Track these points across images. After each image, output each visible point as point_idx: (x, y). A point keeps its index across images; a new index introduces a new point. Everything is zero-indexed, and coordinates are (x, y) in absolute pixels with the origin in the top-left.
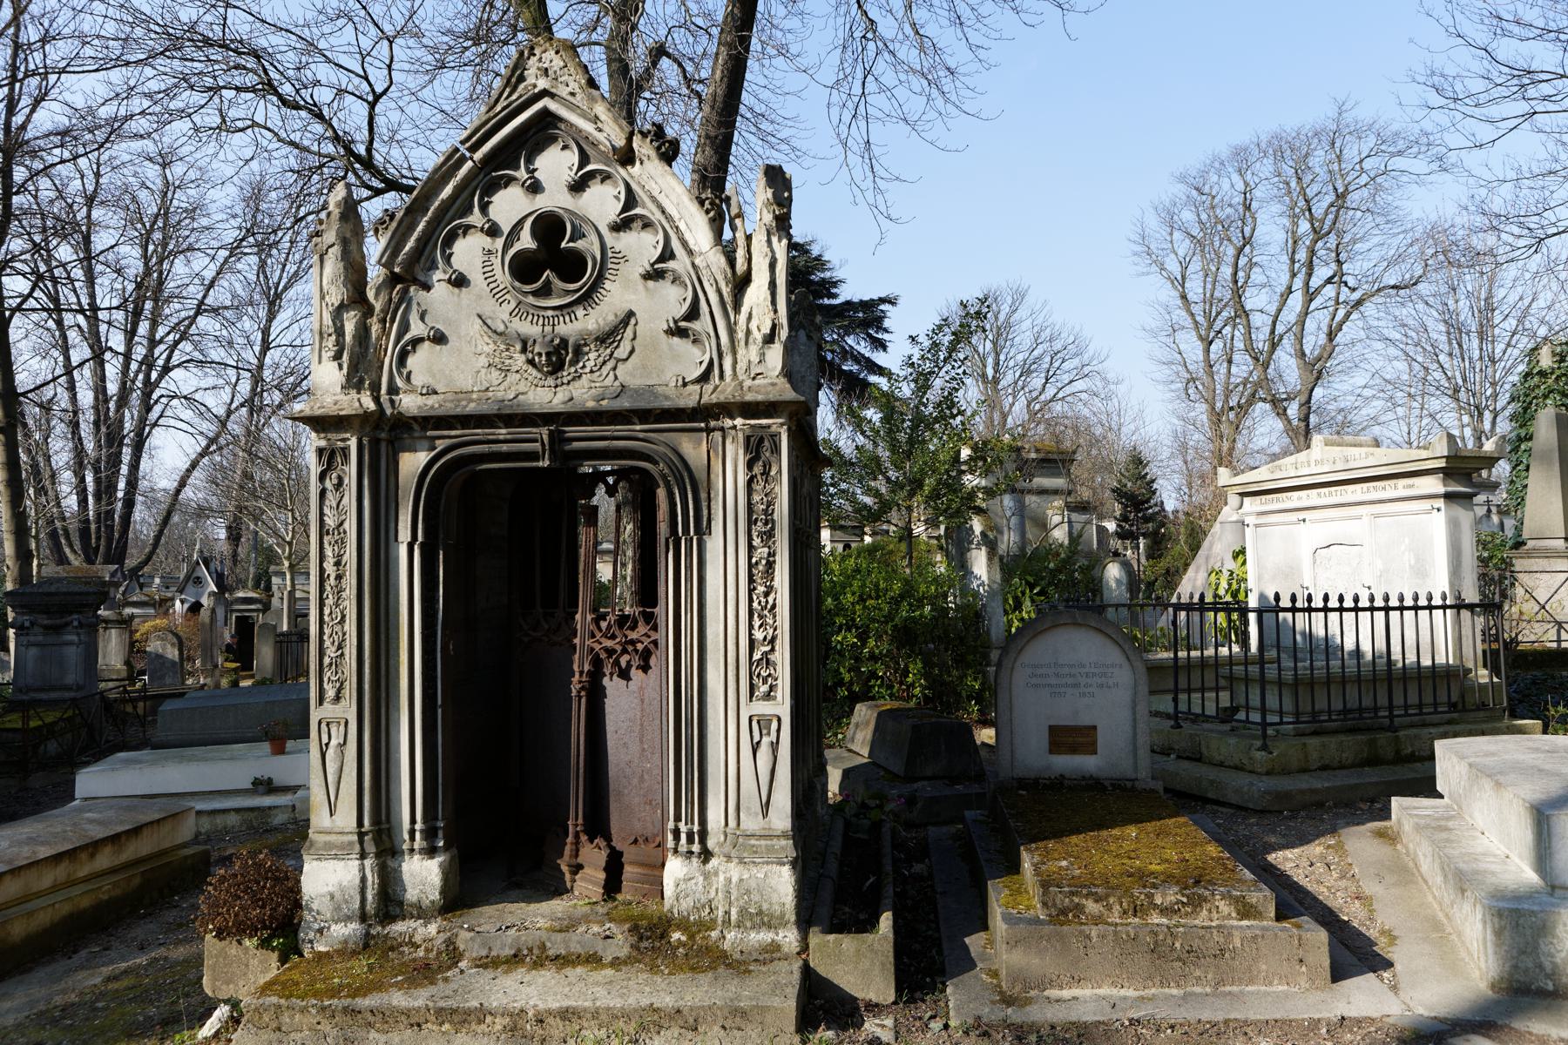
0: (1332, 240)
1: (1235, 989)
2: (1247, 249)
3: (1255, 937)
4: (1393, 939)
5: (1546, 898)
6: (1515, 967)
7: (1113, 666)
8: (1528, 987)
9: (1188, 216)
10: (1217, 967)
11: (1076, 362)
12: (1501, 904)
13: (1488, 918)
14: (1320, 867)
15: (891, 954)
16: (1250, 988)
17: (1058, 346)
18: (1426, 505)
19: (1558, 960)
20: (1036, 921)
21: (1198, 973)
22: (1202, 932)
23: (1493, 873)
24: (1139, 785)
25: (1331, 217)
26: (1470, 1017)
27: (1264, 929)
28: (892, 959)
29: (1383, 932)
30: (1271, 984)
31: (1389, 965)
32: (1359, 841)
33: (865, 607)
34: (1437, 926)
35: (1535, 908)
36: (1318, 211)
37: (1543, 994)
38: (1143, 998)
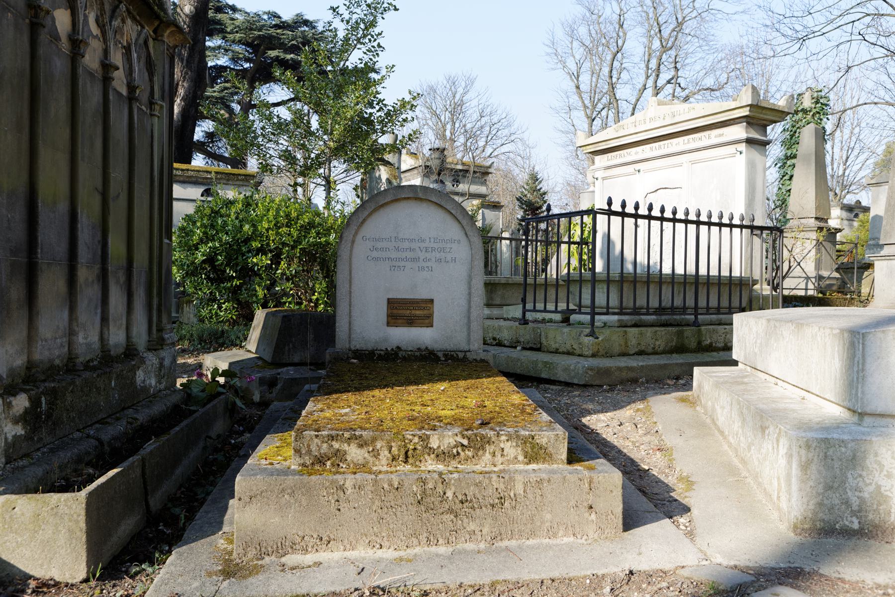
0: (672, 53)
1: (513, 543)
2: (619, 55)
3: (540, 482)
4: (690, 484)
5: (855, 428)
6: (820, 504)
7: (452, 241)
8: (839, 529)
9: (583, 31)
10: (495, 519)
11: (506, 132)
12: (810, 435)
13: (795, 449)
14: (628, 427)
15: (82, 518)
16: (531, 542)
17: (495, 120)
18: (731, 149)
19: (866, 495)
20: (287, 472)
21: (472, 526)
22: (481, 477)
23: (794, 411)
24: (470, 356)
25: (672, 39)
26: (773, 564)
27: (553, 472)
28: (83, 525)
29: (681, 479)
30: (555, 535)
31: (686, 509)
32: (664, 407)
33: (277, 234)
34: (733, 471)
35: (846, 437)
36: (666, 33)
37: (848, 533)
38: (401, 559)
